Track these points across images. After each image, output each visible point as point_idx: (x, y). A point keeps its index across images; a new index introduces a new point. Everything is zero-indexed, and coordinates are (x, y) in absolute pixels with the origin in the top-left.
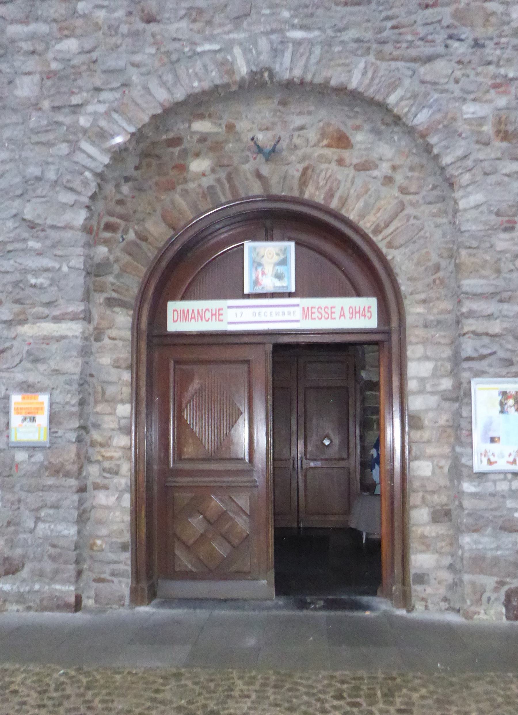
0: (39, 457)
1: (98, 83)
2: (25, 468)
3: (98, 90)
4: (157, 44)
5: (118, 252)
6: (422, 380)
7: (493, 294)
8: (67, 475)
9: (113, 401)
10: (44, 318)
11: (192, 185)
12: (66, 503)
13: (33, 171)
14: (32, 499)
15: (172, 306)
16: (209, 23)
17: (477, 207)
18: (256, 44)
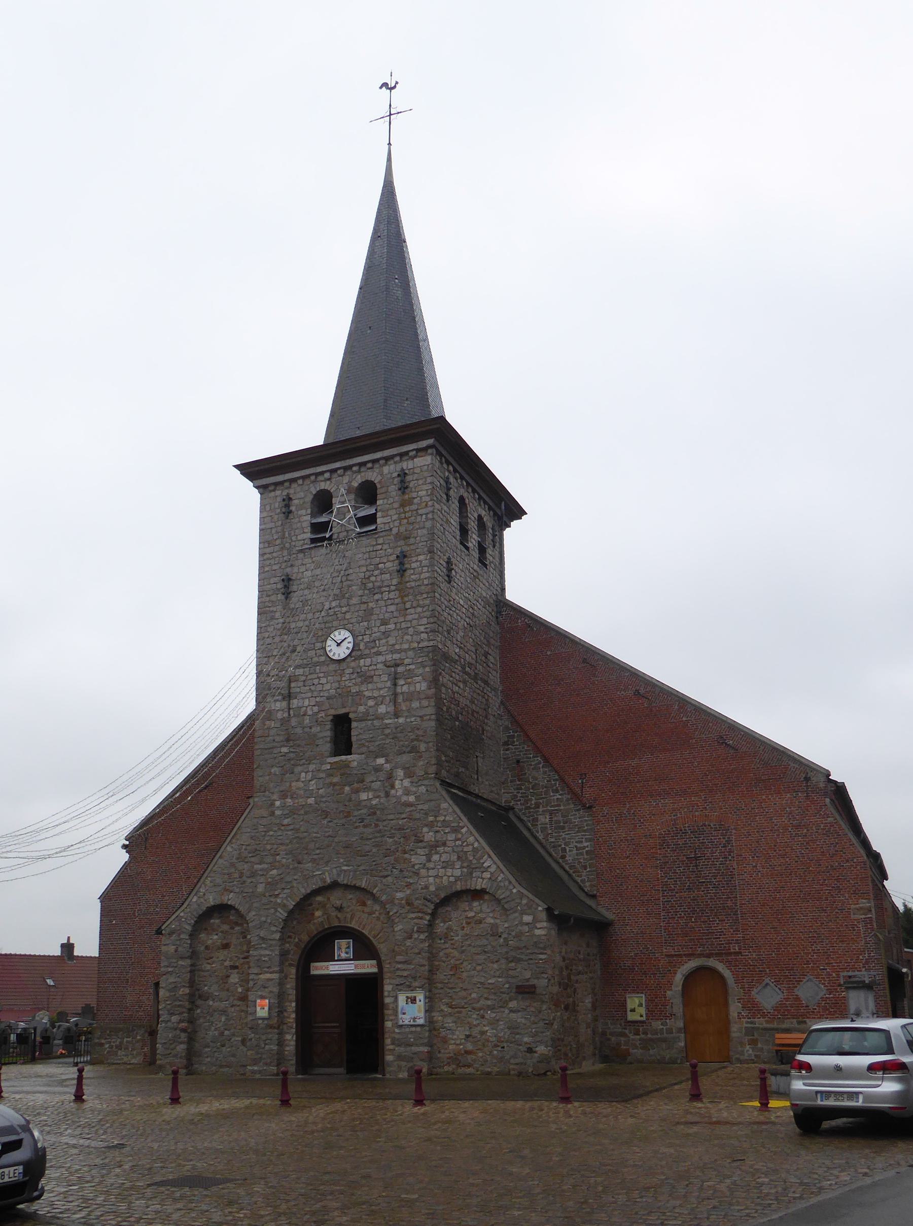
0: (266, 1022)
1: (283, 887)
2: (262, 1026)
3: (284, 889)
4: (302, 872)
5: (292, 947)
6: (389, 992)
7: (406, 962)
8: (275, 1028)
9: (291, 1002)
10: (267, 972)
11: (315, 921)
12: (275, 1038)
13: (263, 919)
14: (264, 1037)
15: (312, 964)
16: (318, 864)
17: (400, 930)
18: (332, 871)
